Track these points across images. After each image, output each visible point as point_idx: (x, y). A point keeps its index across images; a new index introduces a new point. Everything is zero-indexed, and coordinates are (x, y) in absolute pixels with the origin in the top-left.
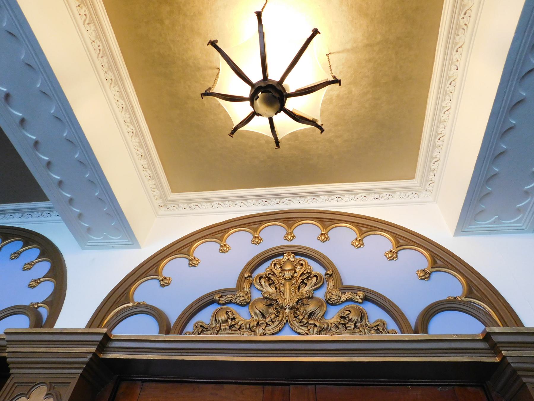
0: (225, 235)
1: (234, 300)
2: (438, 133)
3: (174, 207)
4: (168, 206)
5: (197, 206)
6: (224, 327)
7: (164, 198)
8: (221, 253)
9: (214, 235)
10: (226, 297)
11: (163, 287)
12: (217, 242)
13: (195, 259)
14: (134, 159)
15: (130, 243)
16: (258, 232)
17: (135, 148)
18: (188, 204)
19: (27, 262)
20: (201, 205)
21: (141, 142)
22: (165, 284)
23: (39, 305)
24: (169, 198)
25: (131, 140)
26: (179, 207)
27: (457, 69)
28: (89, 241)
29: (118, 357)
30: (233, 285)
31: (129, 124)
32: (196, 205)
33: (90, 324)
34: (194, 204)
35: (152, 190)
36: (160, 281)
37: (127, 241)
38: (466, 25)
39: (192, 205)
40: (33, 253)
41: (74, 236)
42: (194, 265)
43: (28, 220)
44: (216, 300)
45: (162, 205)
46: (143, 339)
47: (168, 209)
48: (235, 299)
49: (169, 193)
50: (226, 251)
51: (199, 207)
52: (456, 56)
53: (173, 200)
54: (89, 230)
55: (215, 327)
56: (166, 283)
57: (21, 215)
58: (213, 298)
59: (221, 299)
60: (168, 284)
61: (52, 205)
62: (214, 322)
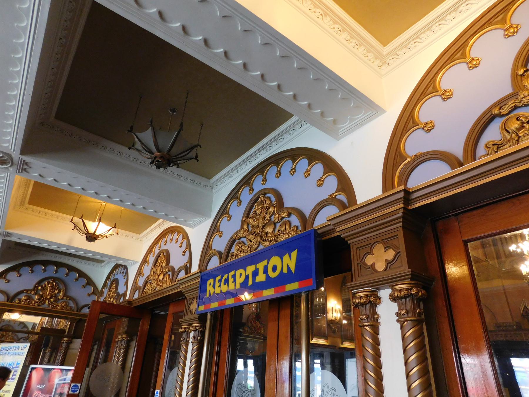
0: (466, 50)
1: (518, 104)
3: (393, 59)
4: (387, 62)
5: (441, 24)
6: (522, 134)
7: (380, 57)
8: (472, 69)
9: (452, 59)
10: (507, 106)
11: (429, 132)
12: (462, 63)
13: (473, 59)
14: (335, 37)
15: (375, 112)
16: (508, 21)
17: (331, 27)
18: (405, 47)
19: (304, 171)
20: (420, 38)
21: (333, 19)
22: (429, 128)
23: (335, 194)
24: (385, 53)
25: (324, 23)
26: (398, 55)
28: (340, 131)
29: (425, 203)
30: (509, 90)
31: (314, 10)
33: (385, 189)
34: (412, 42)
35: (365, 57)
36: (423, 128)
37: (371, 112)
39: (410, 45)
40: (303, 163)
41: (326, 133)
42: (474, 66)
43: (294, 135)
44: (496, 114)
45: (380, 64)
46: (440, 180)
47: (388, 64)
48: (521, 102)
49: (382, 49)
50: (477, 65)
51: (419, 42)
53: (389, 53)
54: (335, 122)
55: (511, 138)
56: (430, 127)
57: (275, 142)
58: (492, 114)
59: (501, 111)
60: (433, 127)
61: (298, 118)
62: (506, 134)
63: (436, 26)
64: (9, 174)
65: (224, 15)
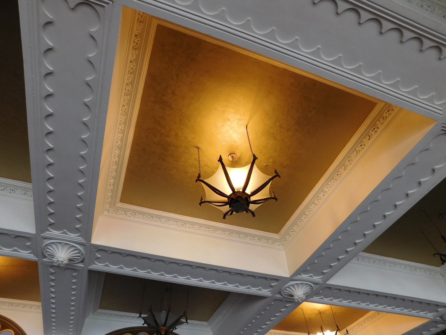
2: (329, 184)
20: (152, 218)
24: (117, 206)
27: (345, 170)
32: (131, 214)
38: (359, 151)
52: (347, 163)
63: (112, 210)
64: (441, 112)
65: (47, 94)
